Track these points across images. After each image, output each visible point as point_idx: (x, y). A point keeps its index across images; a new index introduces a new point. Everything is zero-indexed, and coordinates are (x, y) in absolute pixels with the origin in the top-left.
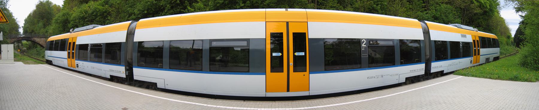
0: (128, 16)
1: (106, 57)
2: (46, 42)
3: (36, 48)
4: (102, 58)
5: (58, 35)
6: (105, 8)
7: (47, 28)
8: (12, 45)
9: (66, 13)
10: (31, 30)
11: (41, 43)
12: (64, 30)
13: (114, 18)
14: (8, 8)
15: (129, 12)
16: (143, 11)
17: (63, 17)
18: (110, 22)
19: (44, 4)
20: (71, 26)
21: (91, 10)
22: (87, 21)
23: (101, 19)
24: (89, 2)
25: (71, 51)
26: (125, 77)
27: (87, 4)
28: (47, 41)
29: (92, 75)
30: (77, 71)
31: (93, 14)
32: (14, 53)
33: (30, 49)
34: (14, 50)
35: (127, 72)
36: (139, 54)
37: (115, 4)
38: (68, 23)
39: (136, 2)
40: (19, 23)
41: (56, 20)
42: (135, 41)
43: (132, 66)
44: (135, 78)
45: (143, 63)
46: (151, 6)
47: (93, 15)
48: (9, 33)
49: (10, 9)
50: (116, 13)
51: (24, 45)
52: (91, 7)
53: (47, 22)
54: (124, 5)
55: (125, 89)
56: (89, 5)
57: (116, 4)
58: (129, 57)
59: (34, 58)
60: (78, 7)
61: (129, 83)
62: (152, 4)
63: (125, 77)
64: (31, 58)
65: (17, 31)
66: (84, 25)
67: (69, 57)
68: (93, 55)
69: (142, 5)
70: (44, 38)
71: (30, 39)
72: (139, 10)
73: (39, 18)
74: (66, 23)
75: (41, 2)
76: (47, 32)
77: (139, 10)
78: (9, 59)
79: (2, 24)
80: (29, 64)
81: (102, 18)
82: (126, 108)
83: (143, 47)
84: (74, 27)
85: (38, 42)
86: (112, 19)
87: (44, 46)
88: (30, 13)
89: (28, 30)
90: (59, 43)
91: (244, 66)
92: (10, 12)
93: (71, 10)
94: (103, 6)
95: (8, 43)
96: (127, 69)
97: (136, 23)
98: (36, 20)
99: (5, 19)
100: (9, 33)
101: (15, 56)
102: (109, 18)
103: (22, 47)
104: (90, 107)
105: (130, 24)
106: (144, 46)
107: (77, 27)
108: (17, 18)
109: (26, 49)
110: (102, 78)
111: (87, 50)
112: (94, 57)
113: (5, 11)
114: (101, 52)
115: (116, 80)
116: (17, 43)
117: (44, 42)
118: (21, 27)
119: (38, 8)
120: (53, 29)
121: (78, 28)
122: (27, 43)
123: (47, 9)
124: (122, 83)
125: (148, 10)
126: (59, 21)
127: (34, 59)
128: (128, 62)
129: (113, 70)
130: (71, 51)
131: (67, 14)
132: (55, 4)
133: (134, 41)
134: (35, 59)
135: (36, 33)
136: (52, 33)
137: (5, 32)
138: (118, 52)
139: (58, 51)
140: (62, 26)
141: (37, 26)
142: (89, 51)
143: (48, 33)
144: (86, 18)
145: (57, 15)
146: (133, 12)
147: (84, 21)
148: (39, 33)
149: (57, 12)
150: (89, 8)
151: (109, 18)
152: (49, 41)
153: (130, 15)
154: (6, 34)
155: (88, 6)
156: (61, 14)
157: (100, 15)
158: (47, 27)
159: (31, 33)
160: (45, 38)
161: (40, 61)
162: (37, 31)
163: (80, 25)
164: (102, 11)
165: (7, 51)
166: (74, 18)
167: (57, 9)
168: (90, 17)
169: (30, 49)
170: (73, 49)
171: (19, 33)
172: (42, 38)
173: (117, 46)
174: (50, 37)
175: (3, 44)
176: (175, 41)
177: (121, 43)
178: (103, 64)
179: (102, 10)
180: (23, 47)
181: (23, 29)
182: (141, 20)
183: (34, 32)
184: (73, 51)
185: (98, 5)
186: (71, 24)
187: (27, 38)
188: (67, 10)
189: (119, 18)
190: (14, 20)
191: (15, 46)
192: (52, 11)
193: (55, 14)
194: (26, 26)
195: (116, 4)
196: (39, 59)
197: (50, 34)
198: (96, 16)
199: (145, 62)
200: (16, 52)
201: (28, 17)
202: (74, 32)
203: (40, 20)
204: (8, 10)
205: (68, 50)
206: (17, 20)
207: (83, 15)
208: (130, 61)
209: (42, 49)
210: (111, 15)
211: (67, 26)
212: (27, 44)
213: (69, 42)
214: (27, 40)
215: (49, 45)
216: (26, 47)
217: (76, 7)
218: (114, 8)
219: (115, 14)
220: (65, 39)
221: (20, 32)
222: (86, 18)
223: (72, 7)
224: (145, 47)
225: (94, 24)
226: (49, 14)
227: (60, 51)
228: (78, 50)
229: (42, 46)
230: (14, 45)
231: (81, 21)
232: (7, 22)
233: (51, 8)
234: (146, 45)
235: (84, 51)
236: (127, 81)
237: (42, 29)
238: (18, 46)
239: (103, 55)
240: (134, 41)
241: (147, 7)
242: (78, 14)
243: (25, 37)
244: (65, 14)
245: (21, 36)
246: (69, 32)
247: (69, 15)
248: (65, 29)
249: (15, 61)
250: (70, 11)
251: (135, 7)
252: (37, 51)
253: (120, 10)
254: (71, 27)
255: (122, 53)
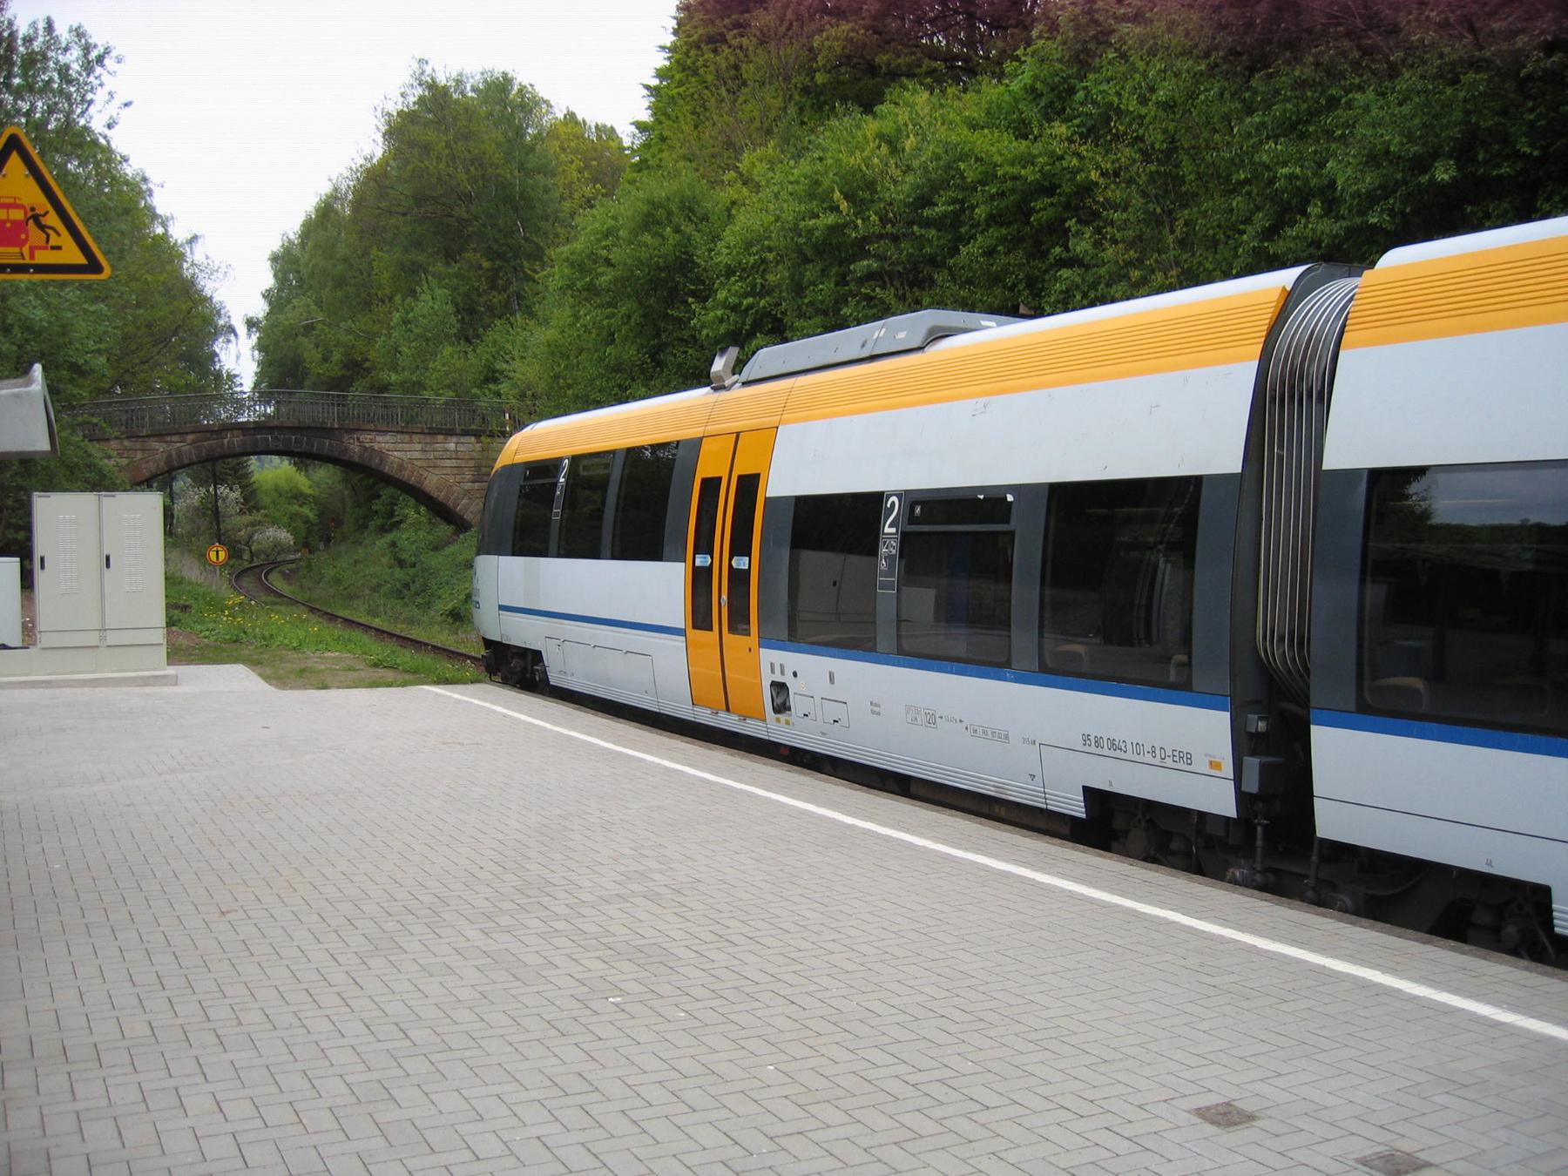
0: (1261, 220)
1: (1054, 616)
2: (481, 469)
3: (383, 530)
4: (1006, 624)
5: (599, 405)
6: (1037, 148)
7: (491, 336)
8: (150, 504)
9: (674, 207)
10: (337, 356)
11: (432, 482)
12: (653, 358)
13: (1131, 244)
14: (97, 125)
15: (1271, 182)
16: (1422, 164)
17: (647, 238)
18: (1094, 286)
19: (468, 109)
20: (721, 320)
21: (908, 169)
22: (871, 276)
23: (1001, 260)
24: (892, 92)
25: (720, 560)
26: (1231, 812)
27: (875, 115)
28: (498, 465)
29: (913, 789)
30: (777, 745)
31: (926, 212)
32: (171, 580)
33: (328, 540)
34: (167, 546)
35: (1252, 764)
36: (1377, 593)
37: (1133, 106)
38: (693, 294)
39: (1342, 75)
40: (210, 286)
41: (580, 266)
42: (1333, 459)
43: (1304, 701)
44: (1331, 822)
45: (1417, 683)
46: (1504, 112)
47: (927, 223)
48: (116, 382)
49: (119, 142)
50: (1144, 194)
51: (267, 500)
52: (909, 143)
53: (493, 285)
54: (1226, 118)
55: (1225, 922)
56: (888, 126)
57: (1150, 110)
58: (1272, 616)
59: (367, 628)
60: (786, 141)
61: (1265, 871)
62: (1510, 85)
63: (1231, 812)
64: (338, 630)
65: (201, 361)
66: (845, 311)
67: (700, 617)
68: (923, 600)
69: (1406, 109)
70: (466, 433)
71: (327, 445)
72: (1373, 159)
73: (418, 244)
74: (674, 296)
75: (432, 86)
76: (491, 377)
77: (1373, 159)
78: (112, 638)
79: (45, 284)
80: (325, 687)
81: (1014, 243)
82: (1240, 1105)
83: (1419, 522)
84: (751, 335)
85: (404, 475)
86: (1110, 252)
87: (470, 508)
88: (326, 189)
89: (310, 353)
90: (602, 485)
91: (156, 677)
92: (129, 170)
93: (728, 167)
94: (1021, 130)
95: (100, 483)
96: (1257, 736)
97: (1341, 287)
98: (384, 263)
99: (66, 239)
100: (116, 382)
101: (178, 610)
102: (1082, 246)
103: (247, 519)
104: (896, 1087)
105: (1290, 300)
106: (1426, 515)
107: (780, 332)
108: (194, 239)
109: (284, 536)
110: (1026, 820)
111: (873, 552)
112: (937, 619)
113: (69, 156)
114: (1002, 571)
115: (1138, 838)
116: (199, 482)
117: (468, 475)
118: (241, 329)
119: (412, 144)
120: (556, 351)
121: (785, 340)
122: (302, 482)
123: (498, 157)
124: (1195, 867)
125: (1463, 153)
126: (606, 277)
127: (365, 639)
128: (1265, 671)
129: (1113, 745)
130: (720, 560)
131: (682, 208)
132: (571, 117)
133: (1329, 463)
134: (379, 631)
135: (384, 388)
136: (542, 387)
137: (75, 368)
138: (1168, 573)
139: (595, 554)
140: (636, 318)
141: (397, 316)
142: (889, 557)
143: (504, 387)
144: (860, 249)
145: (591, 222)
146: (1314, 182)
147: (842, 281)
148: (420, 386)
149: (588, 191)
150: (895, 149)
151: (1082, 246)
152: (511, 469)
153: (1288, 209)
154: (83, 392)
155: (881, 136)
156: (624, 208)
157: (992, 219)
158: (496, 333)
159: (342, 383)
160: (477, 435)
161: (428, 660)
162: (394, 368)
163: (801, 315)
164: (1015, 178)
165: (96, 562)
166: (748, 245)
167: (585, 160)
168: (895, 239)
169: (328, 540)
170: (741, 546)
171: (220, 381)
172: (450, 433)
173: (1162, 511)
174: (519, 425)
175: (50, 486)
176: (1467, 475)
177: (1195, 482)
178: (1017, 681)
179: (1015, 170)
180: (257, 516)
181: (261, 346)
182: (1397, 258)
183: (368, 370)
184: (741, 563)
185: (973, 126)
186: (725, 305)
187: (299, 429)
188: (687, 175)
189: (1182, 243)
190: (166, 255)
191: (179, 507)
192: (540, 178)
193: (567, 205)
194: (291, 317)
195: (1150, 110)
196: (416, 633)
197: (522, 396)
198: (955, 227)
199: (1438, 676)
200: (192, 572)
201: (309, 228)
202: (746, 384)
203: (420, 257)
204: (108, 150)
205: (696, 552)
206: (198, 254)
207: (831, 219)
208: (1280, 655)
209: (448, 543)
210: (1096, 215)
211: (682, 323)
212: (298, 497)
213: (704, 470)
214: (303, 458)
215: (514, 500)
216: (292, 522)
217: (771, 149)
218: (1127, 151)
219: (1137, 201)
220: (664, 446)
221: (231, 377)
222: (860, 249)
223: (730, 145)
224: (1437, 520)
225: (940, 304)
226: (516, 210)
227: (614, 557)
228: (785, 554)
229: (442, 511)
230: (171, 496)
231: (811, 272)
232: (94, 266)
233: (532, 149)
234: (1447, 508)
235: (841, 557)
236: (1244, 850)
237: (447, 350)
238: (212, 512)
239: (1025, 592)
240: (1329, 463)
241: (1458, 115)
242: (790, 209)
243: (280, 428)
244: (661, 213)
245: (239, 413)
246: (698, 376)
247: (705, 218)
248: (661, 348)
249: (176, 655)
250: (714, 183)
251: (1329, 133)
252: (401, 563)
253: (1187, 168)
254: (722, 330)
255: (1211, 575)
